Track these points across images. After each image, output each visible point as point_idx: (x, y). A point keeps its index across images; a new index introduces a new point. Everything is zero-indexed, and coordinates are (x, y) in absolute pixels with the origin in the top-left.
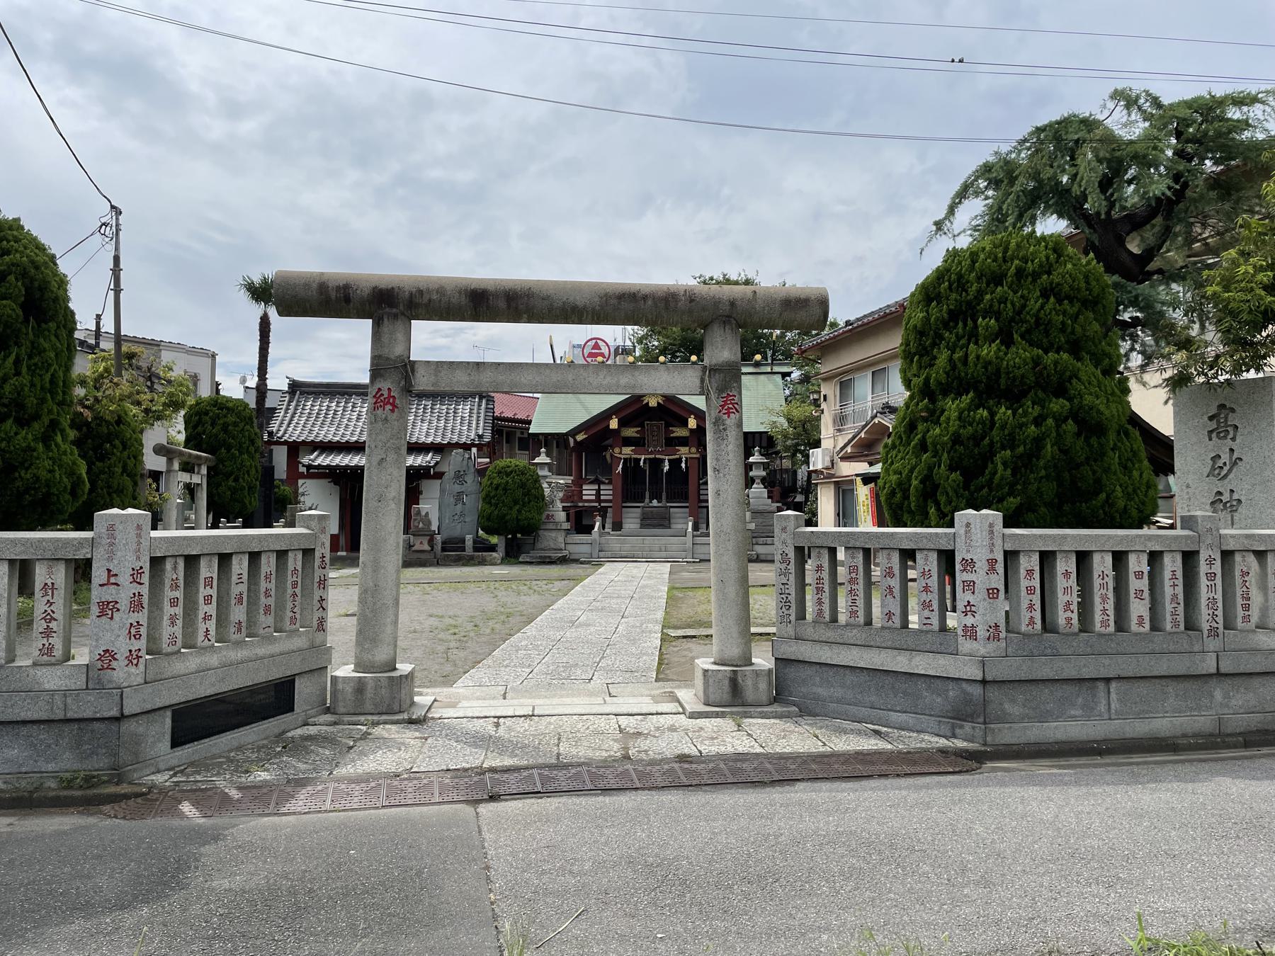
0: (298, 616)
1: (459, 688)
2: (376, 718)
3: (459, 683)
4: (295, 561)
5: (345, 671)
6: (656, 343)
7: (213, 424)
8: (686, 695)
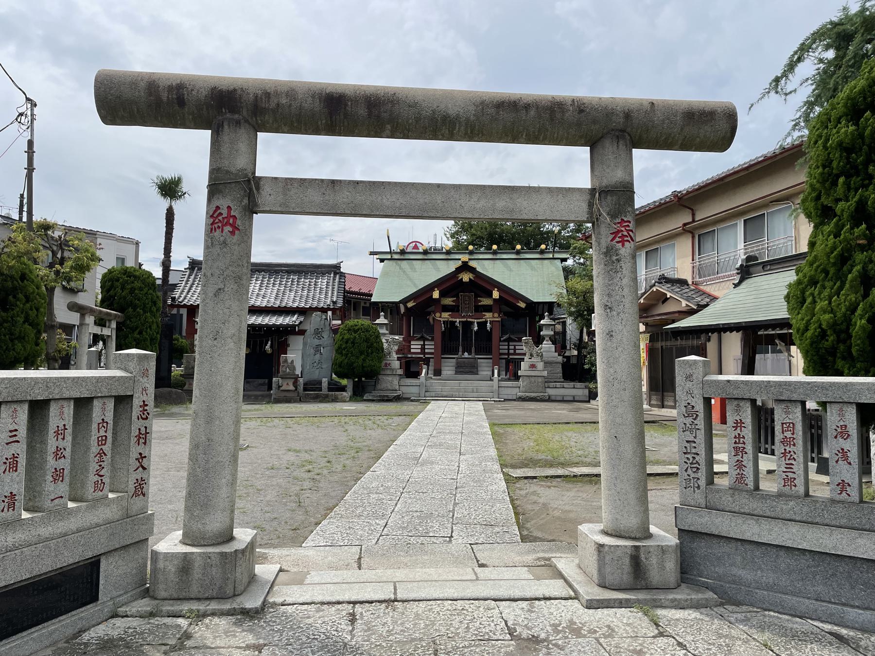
0: (106, 480)
1: (311, 550)
2: (201, 607)
3: (309, 543)
4: (102, 412)
5: (169, 543)
6: (465, 237)
7: (123, 289)
8: (565, 564)
